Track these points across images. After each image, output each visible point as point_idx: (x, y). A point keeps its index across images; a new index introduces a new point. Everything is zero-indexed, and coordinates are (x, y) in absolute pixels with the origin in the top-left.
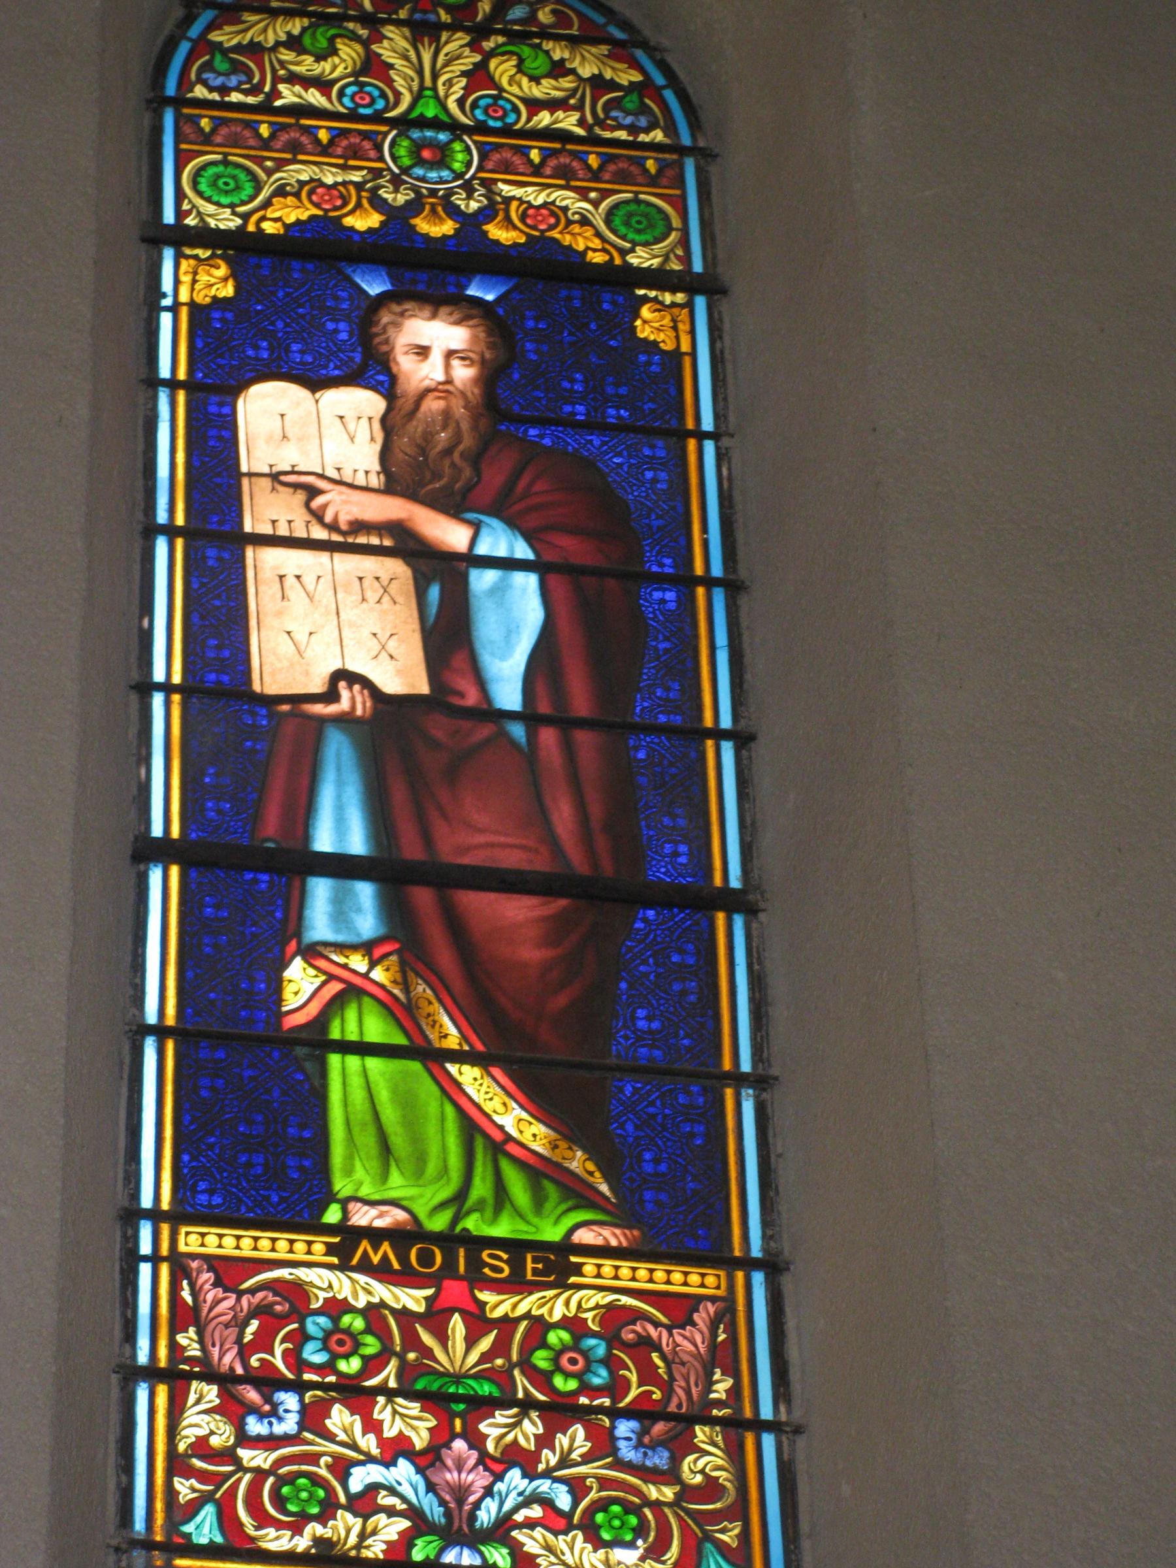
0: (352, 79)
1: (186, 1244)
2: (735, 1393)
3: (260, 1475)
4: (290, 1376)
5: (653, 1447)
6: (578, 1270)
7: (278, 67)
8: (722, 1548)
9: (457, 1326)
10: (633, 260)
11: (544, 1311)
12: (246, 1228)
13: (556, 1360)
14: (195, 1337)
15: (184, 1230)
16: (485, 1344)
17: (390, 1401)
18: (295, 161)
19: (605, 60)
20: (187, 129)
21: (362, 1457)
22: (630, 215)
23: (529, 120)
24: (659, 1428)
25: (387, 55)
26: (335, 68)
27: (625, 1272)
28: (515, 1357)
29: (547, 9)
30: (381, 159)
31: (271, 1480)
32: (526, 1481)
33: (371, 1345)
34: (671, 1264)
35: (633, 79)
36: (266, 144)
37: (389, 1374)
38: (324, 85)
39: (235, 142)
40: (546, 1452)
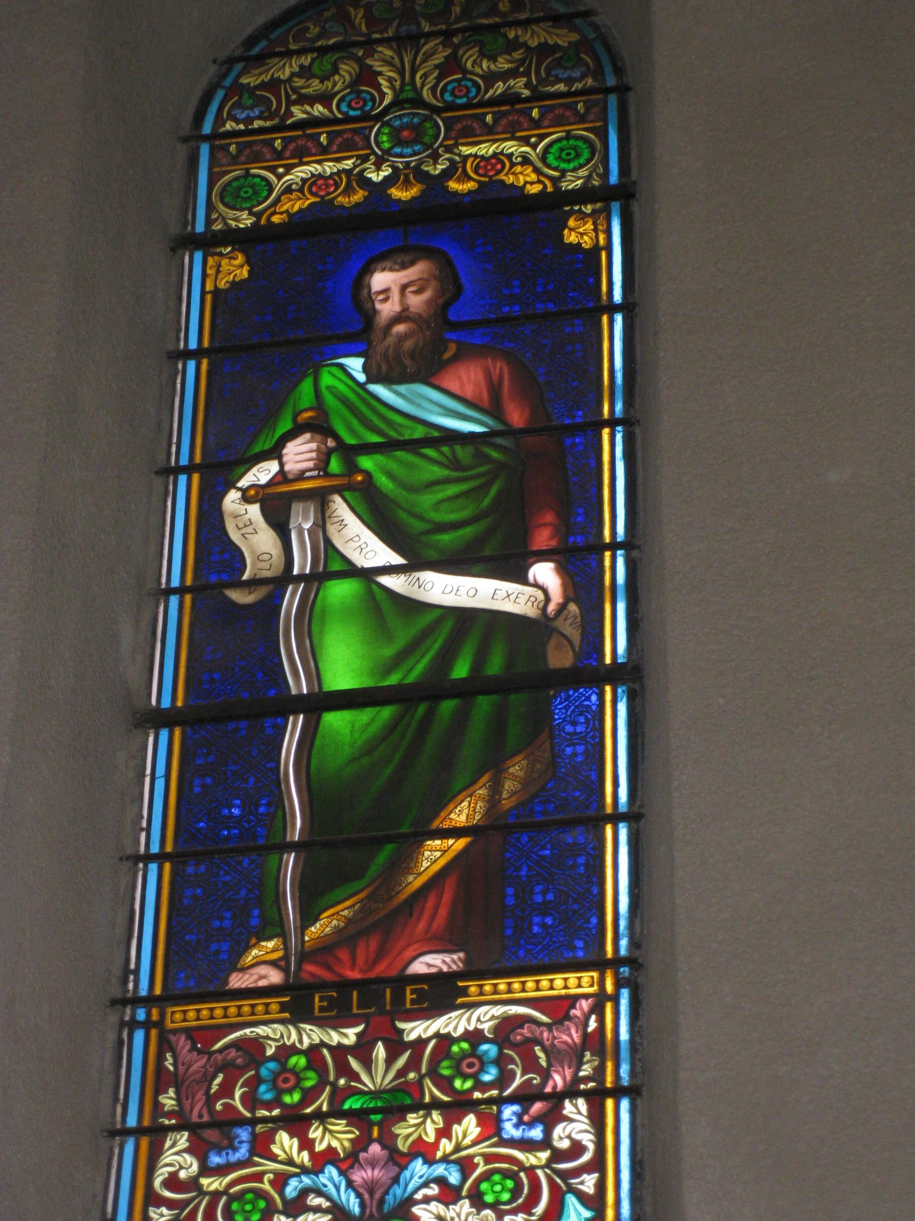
0: (348, 90)
2: (600, 1071)
4: (248, 1115)
5: (531, 1125)
6: (464, 992)
8: (582, 1198)
9: (380, 1051)
10: (564, 185)
11: (450, 1029)
12: (271, 996)
15: (170, 1010)
19: (549, 29)
20: (220, 155)
21: (298, 1170)
22: (562, 150)
23: (486, 92)
24: (537, 1107)
25: (377, 66)
26: (335, 85)
28: (424, 1071)
30: (369, 147)
31: (224, 1199)
32: (426, 1166)
34: (211, 1002)
35: (572, 39)
36: (279, 155)
37: (323, 1103)
38: (325, 99)
39: (257, 158)
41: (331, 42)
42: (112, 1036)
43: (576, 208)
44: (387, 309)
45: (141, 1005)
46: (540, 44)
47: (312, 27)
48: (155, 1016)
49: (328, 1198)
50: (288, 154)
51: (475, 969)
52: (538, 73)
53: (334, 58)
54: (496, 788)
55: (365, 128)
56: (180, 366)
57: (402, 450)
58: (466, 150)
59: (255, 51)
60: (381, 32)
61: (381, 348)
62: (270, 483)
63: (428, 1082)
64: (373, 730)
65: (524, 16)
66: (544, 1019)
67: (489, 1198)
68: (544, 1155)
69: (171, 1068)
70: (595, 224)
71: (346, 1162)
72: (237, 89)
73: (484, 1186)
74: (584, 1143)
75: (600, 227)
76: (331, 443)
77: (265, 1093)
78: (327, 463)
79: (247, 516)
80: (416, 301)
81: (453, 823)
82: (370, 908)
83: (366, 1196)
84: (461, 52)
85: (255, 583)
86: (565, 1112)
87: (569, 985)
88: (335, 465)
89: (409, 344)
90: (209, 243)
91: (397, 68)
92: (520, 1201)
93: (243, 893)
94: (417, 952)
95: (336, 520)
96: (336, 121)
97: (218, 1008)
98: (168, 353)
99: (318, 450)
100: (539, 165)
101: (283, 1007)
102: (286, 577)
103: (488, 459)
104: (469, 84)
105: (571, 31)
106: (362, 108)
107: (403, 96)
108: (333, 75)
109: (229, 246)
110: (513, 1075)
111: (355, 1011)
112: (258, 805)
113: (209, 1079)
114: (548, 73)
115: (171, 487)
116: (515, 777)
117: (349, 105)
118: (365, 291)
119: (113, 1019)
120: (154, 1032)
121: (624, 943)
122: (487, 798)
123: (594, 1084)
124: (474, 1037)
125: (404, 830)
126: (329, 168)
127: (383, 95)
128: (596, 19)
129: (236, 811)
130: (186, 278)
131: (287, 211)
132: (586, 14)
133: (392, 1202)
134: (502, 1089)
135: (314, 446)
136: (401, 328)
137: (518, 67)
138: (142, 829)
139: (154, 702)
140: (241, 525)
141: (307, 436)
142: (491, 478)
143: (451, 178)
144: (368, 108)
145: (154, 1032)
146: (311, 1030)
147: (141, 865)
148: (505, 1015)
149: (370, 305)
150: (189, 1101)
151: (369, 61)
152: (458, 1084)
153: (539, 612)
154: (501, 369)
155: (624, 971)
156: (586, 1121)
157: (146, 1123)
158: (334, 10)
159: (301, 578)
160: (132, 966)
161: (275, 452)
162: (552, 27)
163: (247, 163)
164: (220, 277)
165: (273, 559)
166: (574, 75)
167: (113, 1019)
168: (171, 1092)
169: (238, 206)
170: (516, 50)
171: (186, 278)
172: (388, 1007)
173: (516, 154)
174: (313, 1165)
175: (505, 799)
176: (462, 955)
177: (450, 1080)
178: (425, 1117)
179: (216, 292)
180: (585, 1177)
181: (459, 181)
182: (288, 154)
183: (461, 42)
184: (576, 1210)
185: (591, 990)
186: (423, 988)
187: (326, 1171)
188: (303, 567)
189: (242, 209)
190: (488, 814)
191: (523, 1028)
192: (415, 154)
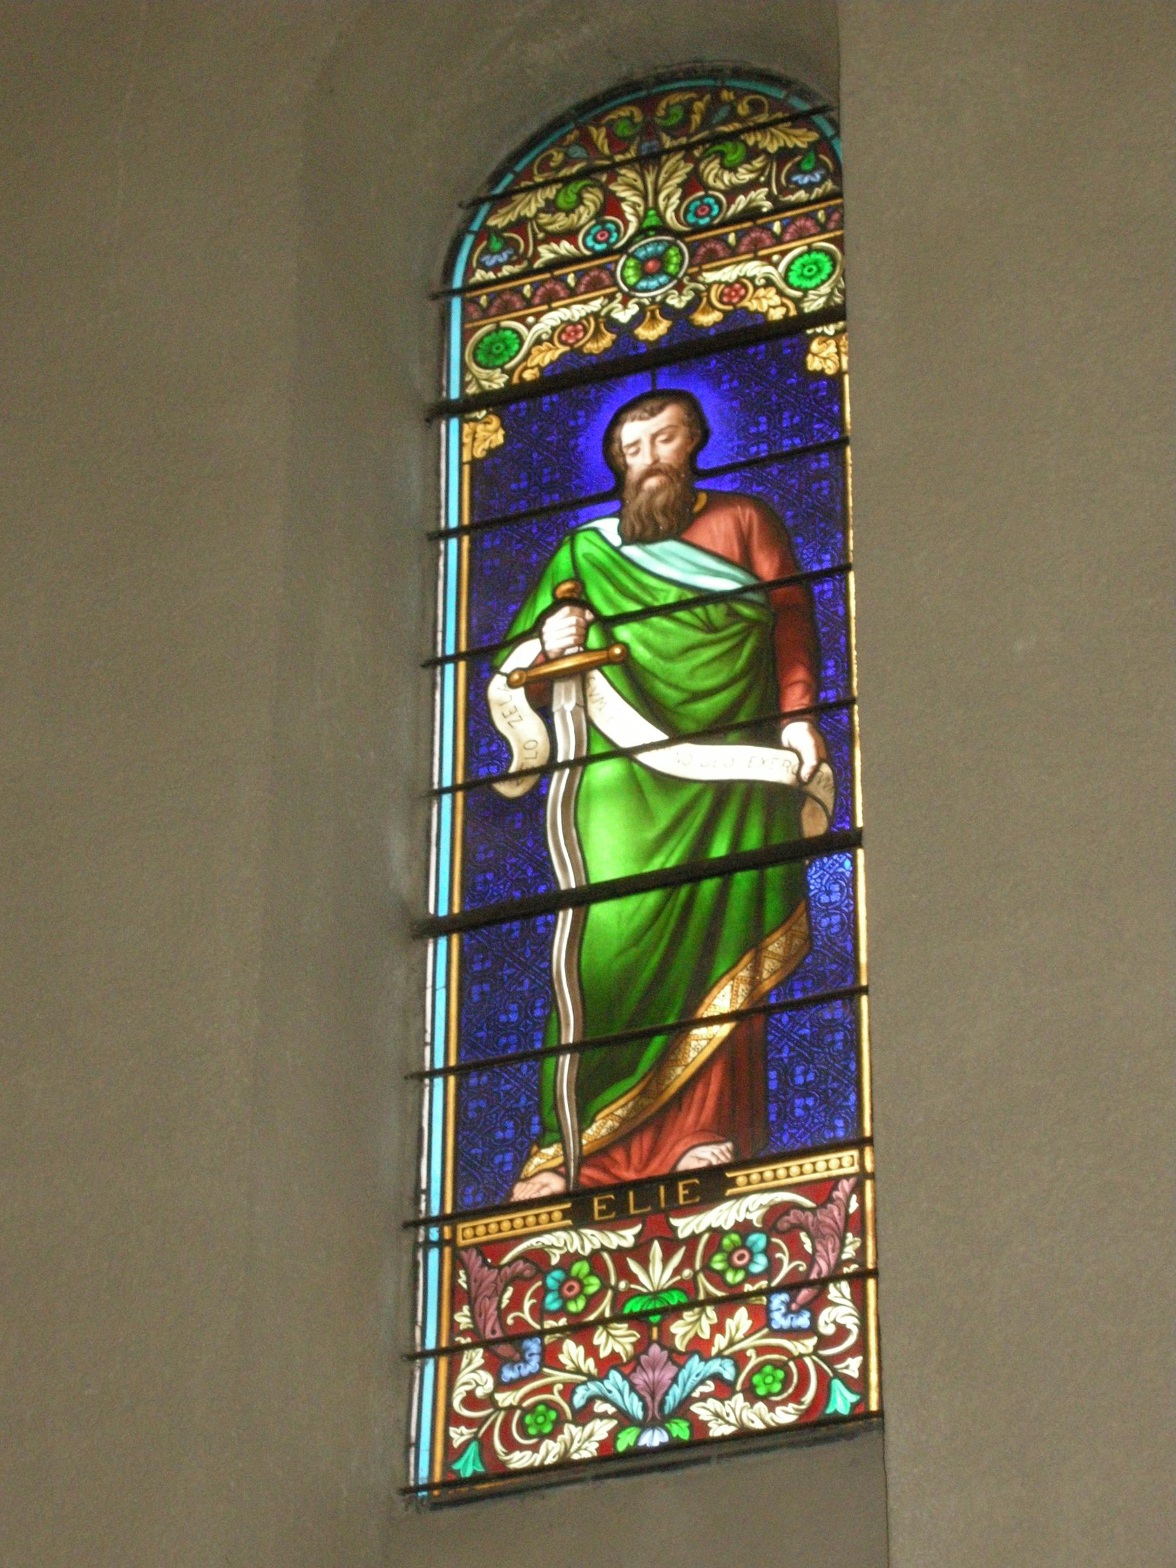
0: (593, 222)
1: (464, 1238)
2: (862, 1251)
3: (511, 1409)
4: (537, 1327)
5: (798, 1312)
6: (732, 1183)
8: (847, 1381)
9: (656, 1249)
14: (468, 1313)
15: (460, 1227)
17: (606, 1328)
18: (551, 309)
20: (471, 309)
21: (584, 1378)
23: (728, 208)
24: (804, 1294)
25: (622, 192)
26: (580, 217)
27: (781, 1172)
28: (698, 1266)
29: (745, 103)
30: (616, 284)
31: (518, 1413)
33: (594, 1285)
35: (811, 139)
36: (529, 304)
38: (570, 234)
39: (506, 309)
40: (718, 1337)
41: (575, 169)
43: (819, 330)
44: (637, 463)
46: (780, 148)
47: (555, 154)
48: (447, 1235)
49: (614, 1404)
50: (537, 300)
54: (756, 968)
55: (610, 263)
58: (709, 277)
59: (499, 190)
60: (622, 153)
63: (701, 1278)
65: (763, 118)
66: (808, 1203)
67: (761, 1391)
69: (465, 1286)
70: (838, 346)
71: (628, 1366)
73: (756, 1379)
75: (843, 349)
77: (552, 1302)
80: (667, 452)
83: (649, 1399)
84: (702, 166)
85: (522, 774)
89: (660, 499)
92: (790, 1390)
93: (523, 1101)
99: (577, 625)
100: (782, 285)
102: (551, 766)
103: (743, 618)
104: (711, 201)
105: (810, 130)
106: (607, 241)
107: (647, 223)
108: (577, 206)
111: (632, 1211)
112: (533, 1008)
118: (616, 446)
120: (447, 1251)
124: (744, 1228)
125: (671, 1021)
126: (577, 312)
127: (626, 223)
129: (514, 1017)
131: (538, 366)
136: (652, 482)
140: (507, 713)
141: (566, 610)
144: (613, 240)
147: (427, 1081)
151: (613, 187)
154: (750, 517)
156: (851, 1304)
159: (567, 764)
161: (536, 631)
162: (793, 127)
164: (476, 444)
168: (466, 1309)
172: (663, 1205)
173: (759, 275)
176: (729, 1145)
177: (722, 1274)
178: (700, 1314)
179: (474, 462)
180: (850, 1361)
181: (704, 312)
182: (537, 300)
184: (842, 1394)
188: (567, 753)
189: (494, 368)
190: (750, 995)
192: (661, 286)
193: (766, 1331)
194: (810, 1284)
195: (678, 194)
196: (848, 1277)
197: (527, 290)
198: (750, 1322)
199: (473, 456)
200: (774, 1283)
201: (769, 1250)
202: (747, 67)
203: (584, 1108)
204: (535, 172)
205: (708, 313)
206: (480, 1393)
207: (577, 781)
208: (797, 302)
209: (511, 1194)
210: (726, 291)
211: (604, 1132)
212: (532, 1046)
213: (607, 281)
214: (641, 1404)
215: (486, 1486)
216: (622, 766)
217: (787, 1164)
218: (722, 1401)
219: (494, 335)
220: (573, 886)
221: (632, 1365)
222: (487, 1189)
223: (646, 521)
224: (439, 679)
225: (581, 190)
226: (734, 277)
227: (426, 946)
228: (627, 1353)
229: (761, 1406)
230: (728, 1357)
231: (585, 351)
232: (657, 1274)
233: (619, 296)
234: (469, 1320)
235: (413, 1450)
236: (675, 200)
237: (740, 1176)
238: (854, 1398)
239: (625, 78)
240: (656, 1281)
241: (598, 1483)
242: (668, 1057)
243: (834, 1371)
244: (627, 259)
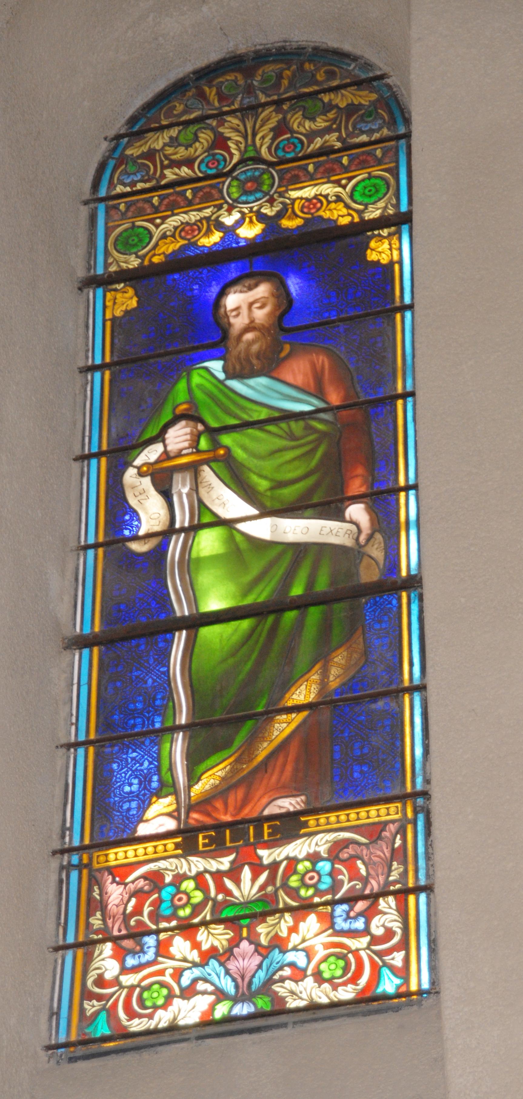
0: (206, 154)
1: (98, 863)
2: (405, 874)
3: (132, 988)
4: (154, 927)
5: (355, 918)
6: (305, 825)
7: (163, 159)
8: (393, 969)
9: (246, 873)
13: (302, 880)
15: (96, 855)
16: (263, 877)
17: (207, 928)
18: (173, 215)
19: (354, 92)
20: (113, 212)
21: (190, 965)
23: (308, 146)
24: (361, 906)
25: (227, 132)
26: (196, 150)
27: (343, 818)
28: (278, 884)
29: (322, 72)
30: (223, 198)
31: (138, 990)
33: (198, 897)
37: (207, 914)
38: (189, 163)
39: (140, 213)
41: (192, 116)
42: (54, 878)
43: (376, 232)
44: (238, 323)
45: (75, 853)
46: (348, 105)
47: (178, 105)
48: (85, 861)
49: (212, 984)
50: (163, 208)
51: (312, 807)
52: (346, 128)
53: (196, 128)
54: (325, 673)
55: (219, 183)
56: (89, 377)
57: (252, 428)
58: (294, 194)
59: (136, 128)
60: (229, 106)
61: (234, 352)
62: (158, 461)
63: (281, 893)
64: (235, 638)
65: (335, 83)
66: (363, 840)
67: (326, 975)
68: (365, 940)
69: (98, 897)
70: (390, 244)
71: (222, 956)
72: (122, 160)
73: (323, 967)
74: (394, 929)
75: (394, 246)
76: (200, 427)
77: (166, 910)
78: (198, 442)
79: (141, 487)
80: (260, 315)
81: (295, 702)
82: (237, 769)
83: (239, 980)
84: (289, 116)
85: (149, 536)
86: (380, 907)
87: (381, 814)
88: (204, 444)
89: (255, 348)
90: (106, 282)
91: (242, 134)
92: (349, 975)
93: (146, 764)
94: (272, 798)
95: (206, 484)
96: (199, 180)
97: (130, 850)
98: (79, 368)
99: (192, 433)
100: (348, 201)
101: (177, 846)
102: (170, 531)
103: (315, 430)
104: (296, 141)
105: (371, 92)
106: (216, 168)
107: (247, 155)
108: (194, 142)
109: (121, 283)
110: (342, 882)
111: (228, 844)
112: (155, 699)
113: (125, 902)
114: (354, 127)
115: (86, 469)
116: (338, 665)
117: (207, 166)
118: (222, 310)
119: (54, 864)
120: (85, 872)
121: (419, 780)
122: (319, 681)
123: (400, 885)
124: (314, 858)
125: (260, 709)
126: (193, 216)
127: (231, 155)
128: (389, 81)
129: (139, 706)
130: (91, 310)
131: (164, 253)
132: (382, 77)
133: (257, 983)
134: (334, 894)
135: (188, 430)
136: (249, 336)
137: (332, 125)
138: (72, 724)
139: (78, 629)
140: (137, 494)
141: (183, 423)
142: (318, 442)
143: (283, 217)
144: (221, 167)
145: (85, 872)
146: (197, 861)
147: (72, 750)
148: (335, 840)
149: (226, 320)
150: (111, 920)
151: (221, 130)
152: (303, 892)
153: (354, 541)
154: (323, 361)
155: (420, 801)
156: (395, 913)
157: (81, 939)
158: (194, 90)
159: (183, 529)
160: (68, 825)
161: (160, 437)
162: (358, 90)
163: (132, 218)
164: (116, 307)
165: (161, 517)
166: (374, 127)
167: (54, 864)
168: (98, 915)
169: (127, 252)
170: (329, 111)
171: (91, 310)
172: (252, 840)
173: (331, 194)
174: (201, 960)
175: (332, 681)
176: (303, 798)
177: (297, 890)
178: (280, 918)
179: (114, 319)
180: (395, 954)
181: (290, 218)
182: (163, 208)
183: (289, 108)
184: (389, 978)
185: (396, 817)
186: (276, 824)
187: (210, 963)
188: (183, 521)
189: (131, 254)
190: (320, 693)
191: (349, 848)
192: (257, 200)
193: (330, 931)
194: (364, 897)
195: (271, 135)
196: (394, 893)
197: (155, 201)
198: (319, 924)
199: (113, 315)
200: (338, 897)
201: (333, 873)
202: (324, 46)
203: (193, 770)
204: (162, 118)
205: (293, 219)
206: (108, 976)
207: (190, 542)
208: (359, 212)
209: (135, 831)
210: (306, 204)
211: (207, 787)
212: (153, 725)
213: (216, 195)
214: (233, 983)
215: (112, 1044)
216: (222, 531)
217: (347, 812)
218: (296, 982)
219: (130, 230)
220: (187, 613)
221: (227, 955)
222: (117, 827)
223: (244, 363)
224: (86, 469)
225: (197, 130)
226: (312, 194)
227: (74, 655)
228: (223, 946)
229: (326, 986)
230: (303, 950)
231: (199, 244)
232: (247, 887)
233: (225, 206)
234: (100, 922)
235: (55, 1017)
236: (268, 140)
237: (311, 820)
238: (398, 981)
239: (232, 52)
240: (246, 892)
241: (200, 1041)
242: (255, 738)
243: (383, 961)
244: (232, 180)
